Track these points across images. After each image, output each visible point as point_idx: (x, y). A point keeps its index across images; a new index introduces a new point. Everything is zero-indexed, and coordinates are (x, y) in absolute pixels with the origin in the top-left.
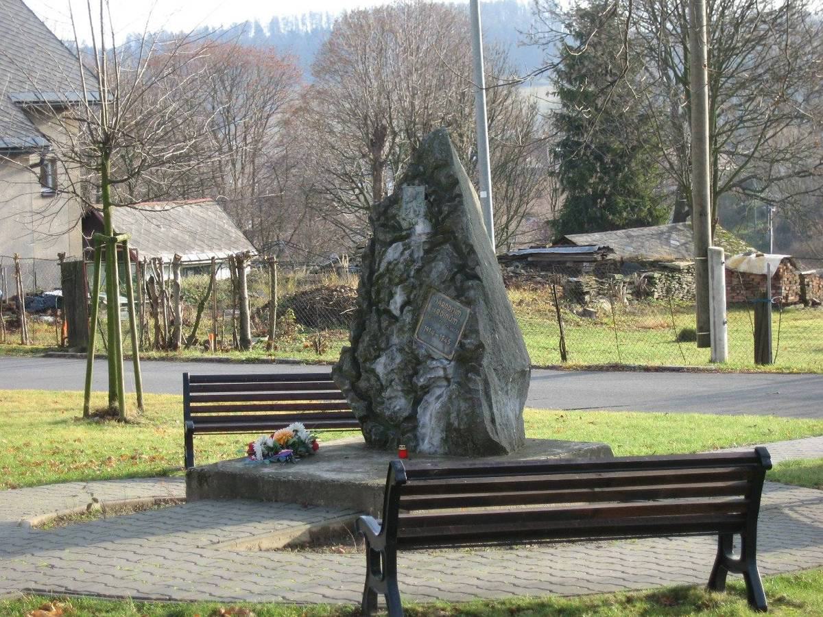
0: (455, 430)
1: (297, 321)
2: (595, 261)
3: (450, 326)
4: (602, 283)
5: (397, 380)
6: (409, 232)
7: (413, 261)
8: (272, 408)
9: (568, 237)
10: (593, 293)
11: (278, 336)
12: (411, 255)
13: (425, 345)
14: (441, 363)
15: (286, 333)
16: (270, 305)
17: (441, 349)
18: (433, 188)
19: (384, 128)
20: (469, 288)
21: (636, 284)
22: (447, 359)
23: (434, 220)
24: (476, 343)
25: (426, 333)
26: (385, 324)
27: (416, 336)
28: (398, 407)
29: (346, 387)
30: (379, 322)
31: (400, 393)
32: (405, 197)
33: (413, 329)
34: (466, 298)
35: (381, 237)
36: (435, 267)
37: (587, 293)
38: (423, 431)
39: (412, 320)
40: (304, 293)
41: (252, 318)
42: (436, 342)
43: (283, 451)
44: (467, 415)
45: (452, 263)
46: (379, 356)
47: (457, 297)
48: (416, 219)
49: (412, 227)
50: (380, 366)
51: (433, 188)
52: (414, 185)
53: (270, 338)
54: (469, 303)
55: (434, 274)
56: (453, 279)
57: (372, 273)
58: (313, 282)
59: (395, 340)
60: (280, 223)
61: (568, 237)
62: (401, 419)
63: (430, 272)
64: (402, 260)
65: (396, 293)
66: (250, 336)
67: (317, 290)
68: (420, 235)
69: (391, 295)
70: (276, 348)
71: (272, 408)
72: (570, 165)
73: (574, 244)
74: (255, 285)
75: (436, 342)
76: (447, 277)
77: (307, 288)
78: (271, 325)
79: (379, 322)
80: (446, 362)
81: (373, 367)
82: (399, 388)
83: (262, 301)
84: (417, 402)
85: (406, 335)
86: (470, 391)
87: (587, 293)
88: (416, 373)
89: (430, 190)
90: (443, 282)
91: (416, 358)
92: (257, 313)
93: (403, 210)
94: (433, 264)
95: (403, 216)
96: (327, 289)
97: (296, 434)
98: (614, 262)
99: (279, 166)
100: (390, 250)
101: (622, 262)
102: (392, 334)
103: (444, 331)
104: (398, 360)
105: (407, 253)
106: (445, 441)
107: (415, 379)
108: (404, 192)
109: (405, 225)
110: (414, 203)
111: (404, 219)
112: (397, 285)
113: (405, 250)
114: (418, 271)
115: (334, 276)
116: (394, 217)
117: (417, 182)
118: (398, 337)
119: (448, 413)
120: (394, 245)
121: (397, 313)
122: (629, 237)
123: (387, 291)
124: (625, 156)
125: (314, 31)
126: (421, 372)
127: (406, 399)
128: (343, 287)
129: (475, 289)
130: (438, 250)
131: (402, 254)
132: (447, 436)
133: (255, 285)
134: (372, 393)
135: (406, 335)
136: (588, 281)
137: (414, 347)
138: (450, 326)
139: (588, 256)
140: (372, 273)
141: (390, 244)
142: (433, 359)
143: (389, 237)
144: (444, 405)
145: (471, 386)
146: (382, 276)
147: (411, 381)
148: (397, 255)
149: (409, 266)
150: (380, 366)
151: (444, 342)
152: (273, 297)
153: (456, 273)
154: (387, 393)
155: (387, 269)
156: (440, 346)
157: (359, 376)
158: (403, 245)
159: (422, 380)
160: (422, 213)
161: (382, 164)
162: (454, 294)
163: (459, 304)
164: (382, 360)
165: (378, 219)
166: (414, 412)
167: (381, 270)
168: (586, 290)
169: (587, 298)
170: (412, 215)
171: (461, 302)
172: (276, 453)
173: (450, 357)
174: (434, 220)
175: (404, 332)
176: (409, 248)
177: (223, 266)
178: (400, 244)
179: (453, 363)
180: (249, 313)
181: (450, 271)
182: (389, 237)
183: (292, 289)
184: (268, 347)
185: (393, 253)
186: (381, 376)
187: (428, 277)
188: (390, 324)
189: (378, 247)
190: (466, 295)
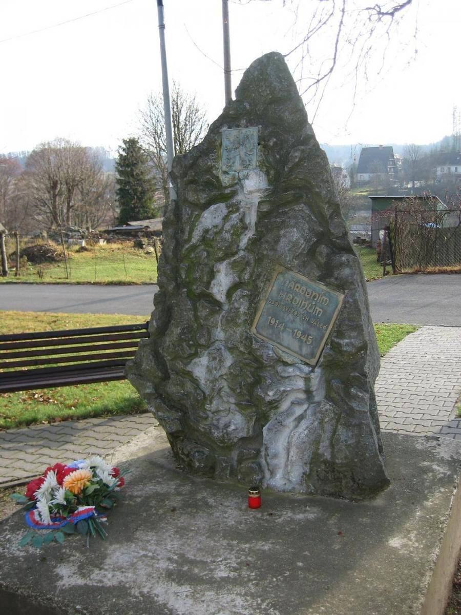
0: (325, 462)
1: (28, 261)
2: (143, 231)
3: (310, 319)
4: (150, 240)
5: (226, 389)
6: (233, 189)
7: (245, 228)
8: (36, 363)
9: (129, 222)
10: (146, 244)
11: (20, 267)
12: (242, 220)
13: (271, 344)
14: (300, 369)
15: (23, 266)
16: (15, 253)
17: (297, 349)
18: (270, 129)
19: (57, 181)
20: (341, 265)
21: (162, 240)
22: (307, 364)
23: (272, 172)
24: (358, 343)
25: (271, 326)
26: (203, 313)
27: (254, 330)
28: (233, 427)
29: (148, 391)
30: (195, 309)
31: (233, 407)
32: (226, 143)
33: (249, 322)
34: (336, 279)
35: (192, 197)
36: (285, 236)
37: (144, 244)
38: (275, 461)
39: (248, 309)
40: (29, 248)
41: (8, 260)
42: (287, 338)
43: (81, 508)
44: (348, 446)
45: (311, 230)
46: (196, 355)
47: (321, 279)
48: (245, 172)
49: (238, 183)
50: (200, 368)
51: (270, 129)
52: (238, 126)
53: (17, 269)
54: (341, 286)
55: (283, 244)
56: (312, 252)
57: (178, 245)
58: (32, 243)
59: (219, 334)
60: (16, 219)
61: (129, 222)
62: (235, 440)
63: (277, 242)
64: (227, 226)
65: (219, 271)
66: (7, 269)
67: (35, 246)
68: (251, 192)
69: (212, 274)
70: (19, 275)
71: (36, 363)
72: (122, 197)
73: (130, 225)
74: (7, 244)
75: (287, 338)
76: (304, 249)
77: (30, 245)
78: (17, 264)
79: (195, 309)
80: (306, 369)
81: (189, 368)
82: (232, 400)
83: (11, 251)
84: (262, 419)
85: (239, 330)
86: (351, 412)
87: (144, 244)
88: (258, 381)
89: (266, 133)
90: (296, 257)
91: (257, 360)
92: (10, 256)
93: (223, 160)
94: (282, 232)
95: (224, 168)
96: (39, 245)
97: (95, 475)
98: (151, 232)
99: (16, 199)
100: (207, 215)
101: (154, 231)
102: (216, 326)
103: (299, 325)
104: (229, 362)
105: (235, 217)
106: (307, 476)
107: (259, 392)
108: (224, 137)
109: (226, 180)
110: (242, 151)
111: (225, 173)
112: (221, 260)
113: (231, 212)
114: (255, 243)
115: (40, 240)
116: (209, 170)
117: (244, 122)
118: (225, 331)
119: (317, 442)
120: (212, 208)
121: (221, 296)
122: (150, 222)
123: (207, 270)
124: (143, 192)
125: (24, 157)
126: (269, 381)
127: (243, 414)
128: (46, 244)
129: (351, 267)
130: (286, 213)
131: (226, 218)
132: (311, 470)
133: (7, 244)
134: (188, 403)
135: (239, 330)
136: (145, 240)
137: (255, 346)
138: (310, 319)
139: (140, 230)
140: (178, 245)
141: (206, 206)
142: (286, 364)
143: (203, 198)
144: (311, 430)
145: (354, 404)
146: (194, 248)
147: (251, 393)
148: (218, 221)
149: (239, 235)
150: (200, 368)
151: (300, 340)
152: (17, 249)
153: (316, 244)
154: (214, 405)
155: (203, 239)
156: (295, 345)
157: (166, 377)
158: (227, 207)
159: (271, 393)
160: (255, 162)
161: (56, 195)
162: (317, 273)
163: (324, 288)
164: (204, 360)
165: (185, 174)
166: (256, 437)
167: (194, 240)
168: (144, 243)
169: (144, 246)
170: (237, 166)
171: (327, 284)
172: (72, 511)
173: (313, 362)
174: (272, 172)
175: (237, 325)
176: (238, 210)
177: (93, 158)
178: (222, 206)
179: (318, 370)
180: (6, 258)
181: (307, 241)
182: (203, 198)
183: (23, 246)
184: (16, 275)
185: (210, 218)
186: (203, 382)
187: (273, 249)
188: (213, 312)
189: (186, 212)
190: (336, 274)
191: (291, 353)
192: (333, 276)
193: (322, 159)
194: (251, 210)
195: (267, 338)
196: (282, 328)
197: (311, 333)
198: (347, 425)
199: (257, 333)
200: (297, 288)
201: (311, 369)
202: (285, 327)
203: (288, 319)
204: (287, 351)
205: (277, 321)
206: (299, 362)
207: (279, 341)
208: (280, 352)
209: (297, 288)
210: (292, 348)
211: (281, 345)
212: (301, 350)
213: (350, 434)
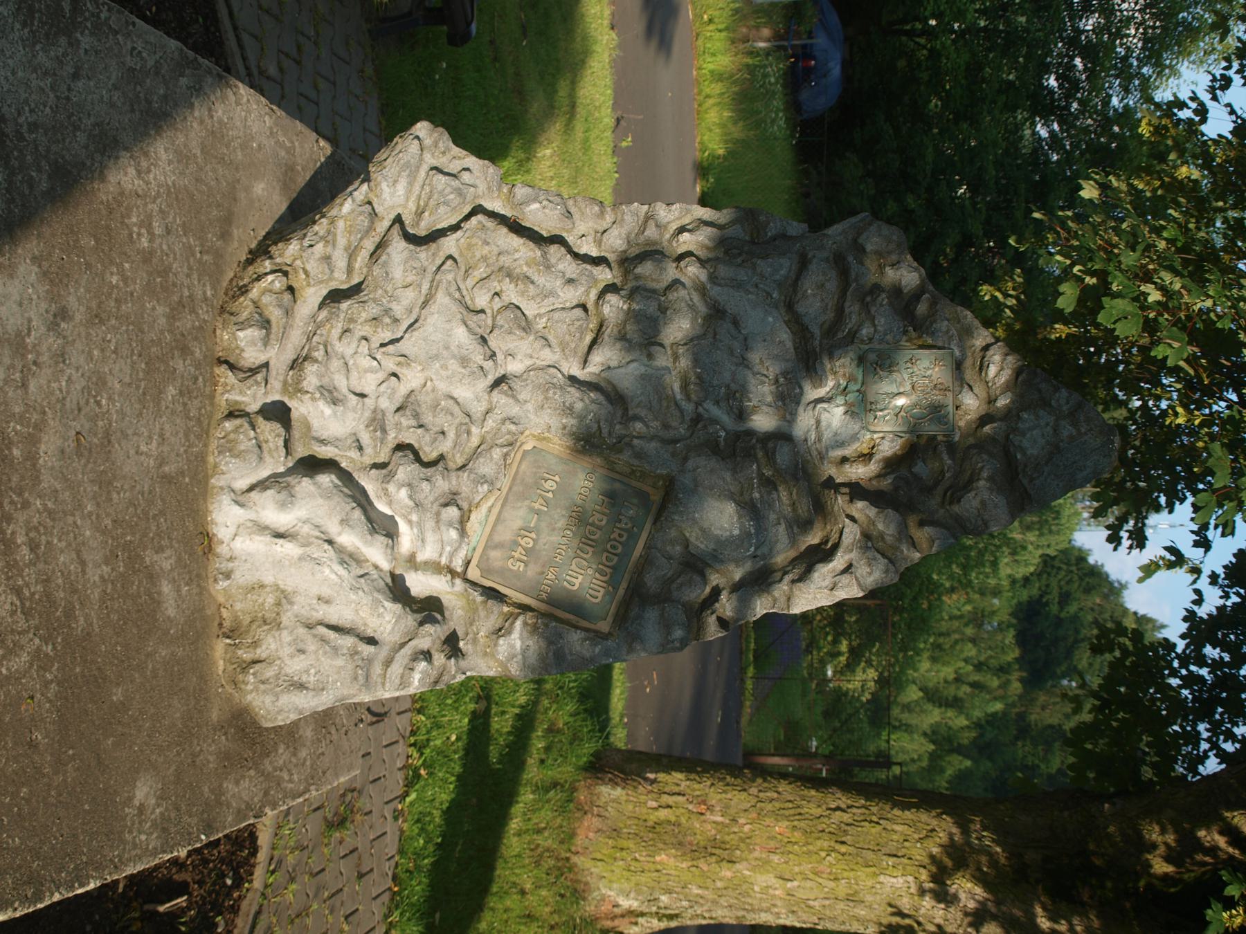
22: (467, 563)
191: (488, 529)
192: (1123, 586)
193: (1106, 597)
194: (382, 703)
195: (517, 472)
196: (537, 506)
197: (531, 566)
198: (13, 681)
199: (525, 452)
200: (620, 536)
201: (459, 570)
202: (538, 512)
203: (556, 517)
204: (492, 519)
205: (550, 495)
206: (473, 544)
207: (511, 498)
208: (489, 504)
209: (620, 536)
210: (500, 528)
211: (503, 506)
212: (496, 547)
213: (249, 697)
